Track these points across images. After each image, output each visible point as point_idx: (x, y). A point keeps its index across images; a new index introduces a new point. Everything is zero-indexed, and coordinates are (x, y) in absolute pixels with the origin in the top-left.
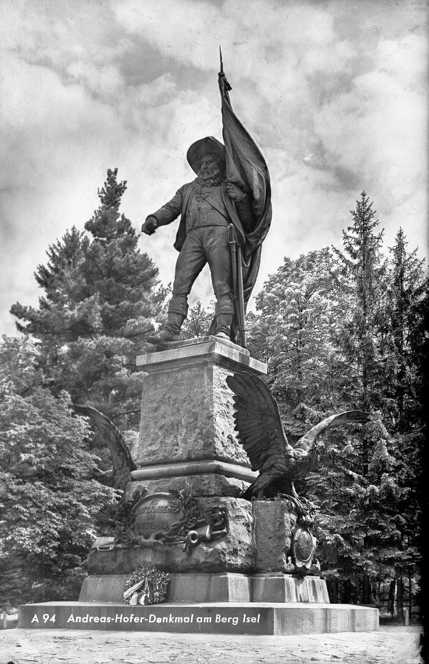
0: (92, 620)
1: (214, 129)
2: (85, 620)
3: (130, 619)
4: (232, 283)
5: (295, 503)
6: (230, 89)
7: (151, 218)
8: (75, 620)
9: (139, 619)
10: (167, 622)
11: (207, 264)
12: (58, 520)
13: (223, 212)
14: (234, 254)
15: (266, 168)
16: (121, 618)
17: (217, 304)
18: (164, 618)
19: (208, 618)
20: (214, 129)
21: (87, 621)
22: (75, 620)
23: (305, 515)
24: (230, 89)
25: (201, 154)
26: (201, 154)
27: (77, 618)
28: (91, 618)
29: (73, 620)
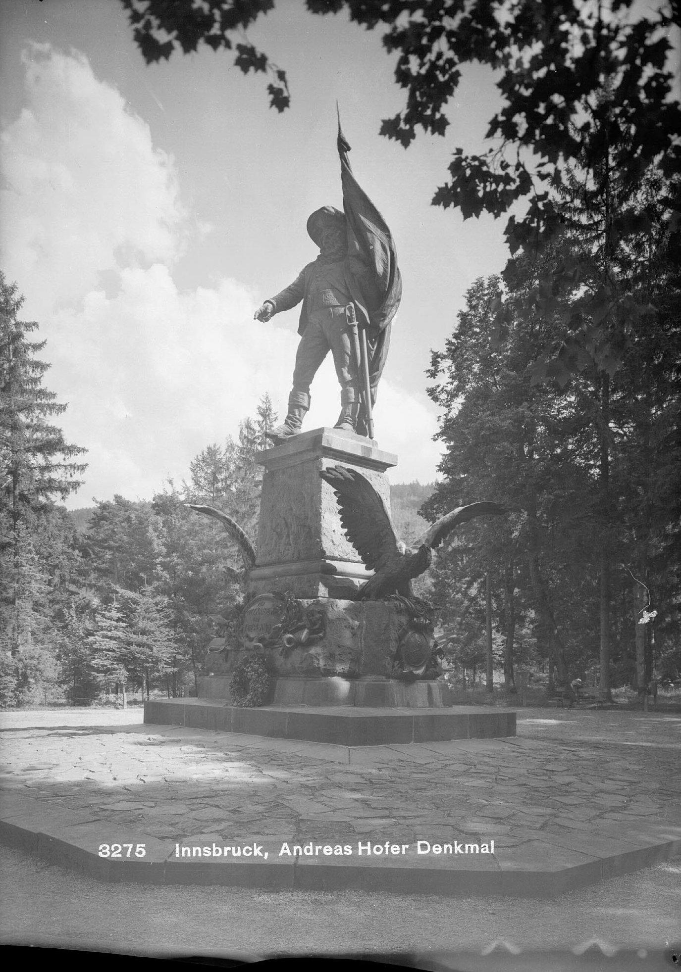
0: (321, 851)
1: (336, 202)
2: (308, 851)
3: (384, 848)
4: (356, 370)
5: (406, 604)
6: (349, 149)
7: (268, 304)
8: (292, 851)
9: (398, 848)
10: (189, 855)
11: (330, 355)
12: (335, 772)
13: (343, 291)
14: (357, 337)
15: (389, 237)
16: (369, 847)
17: (416, 576)
18: (446, 846)
19: (472, 846)
20: (336, 202)
21: (311, 853)
22: (292, 851)
23: (417, 617)
24: (349, 149)
25: (320, 224)
26: (320, 224)
27: (295, 848)
28: (317, 848)
29: (288, 851)
